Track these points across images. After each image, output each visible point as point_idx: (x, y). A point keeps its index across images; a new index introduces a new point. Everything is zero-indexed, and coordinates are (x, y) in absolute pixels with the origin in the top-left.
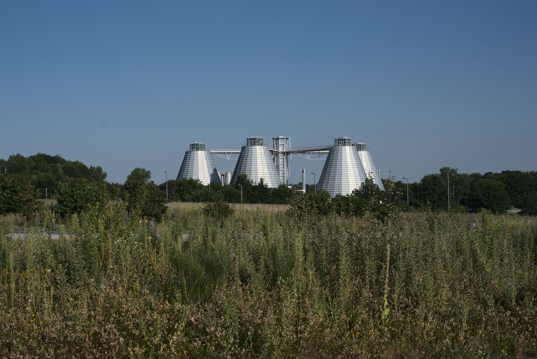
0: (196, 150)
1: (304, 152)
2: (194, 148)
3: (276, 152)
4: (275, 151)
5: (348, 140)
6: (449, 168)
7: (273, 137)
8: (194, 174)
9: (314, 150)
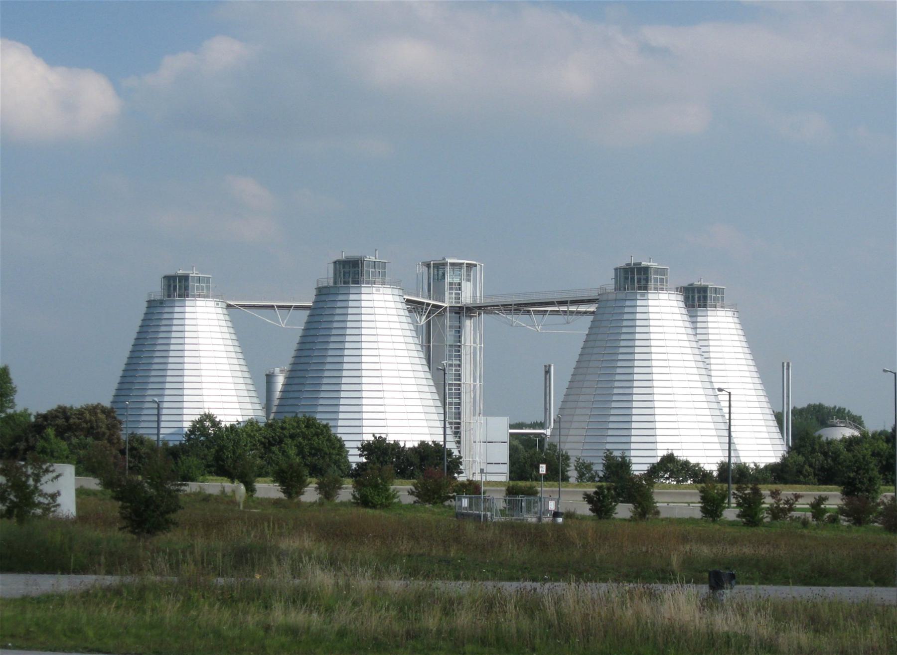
0: (180, 296)
1: (520, 308)
2: (175, 289)
3: (434, 306)
4: (428, 304)
5: (657, 271)
6: (845, 409)
7: (427, 260)
8: (186, 398)
9: (551, 304)
